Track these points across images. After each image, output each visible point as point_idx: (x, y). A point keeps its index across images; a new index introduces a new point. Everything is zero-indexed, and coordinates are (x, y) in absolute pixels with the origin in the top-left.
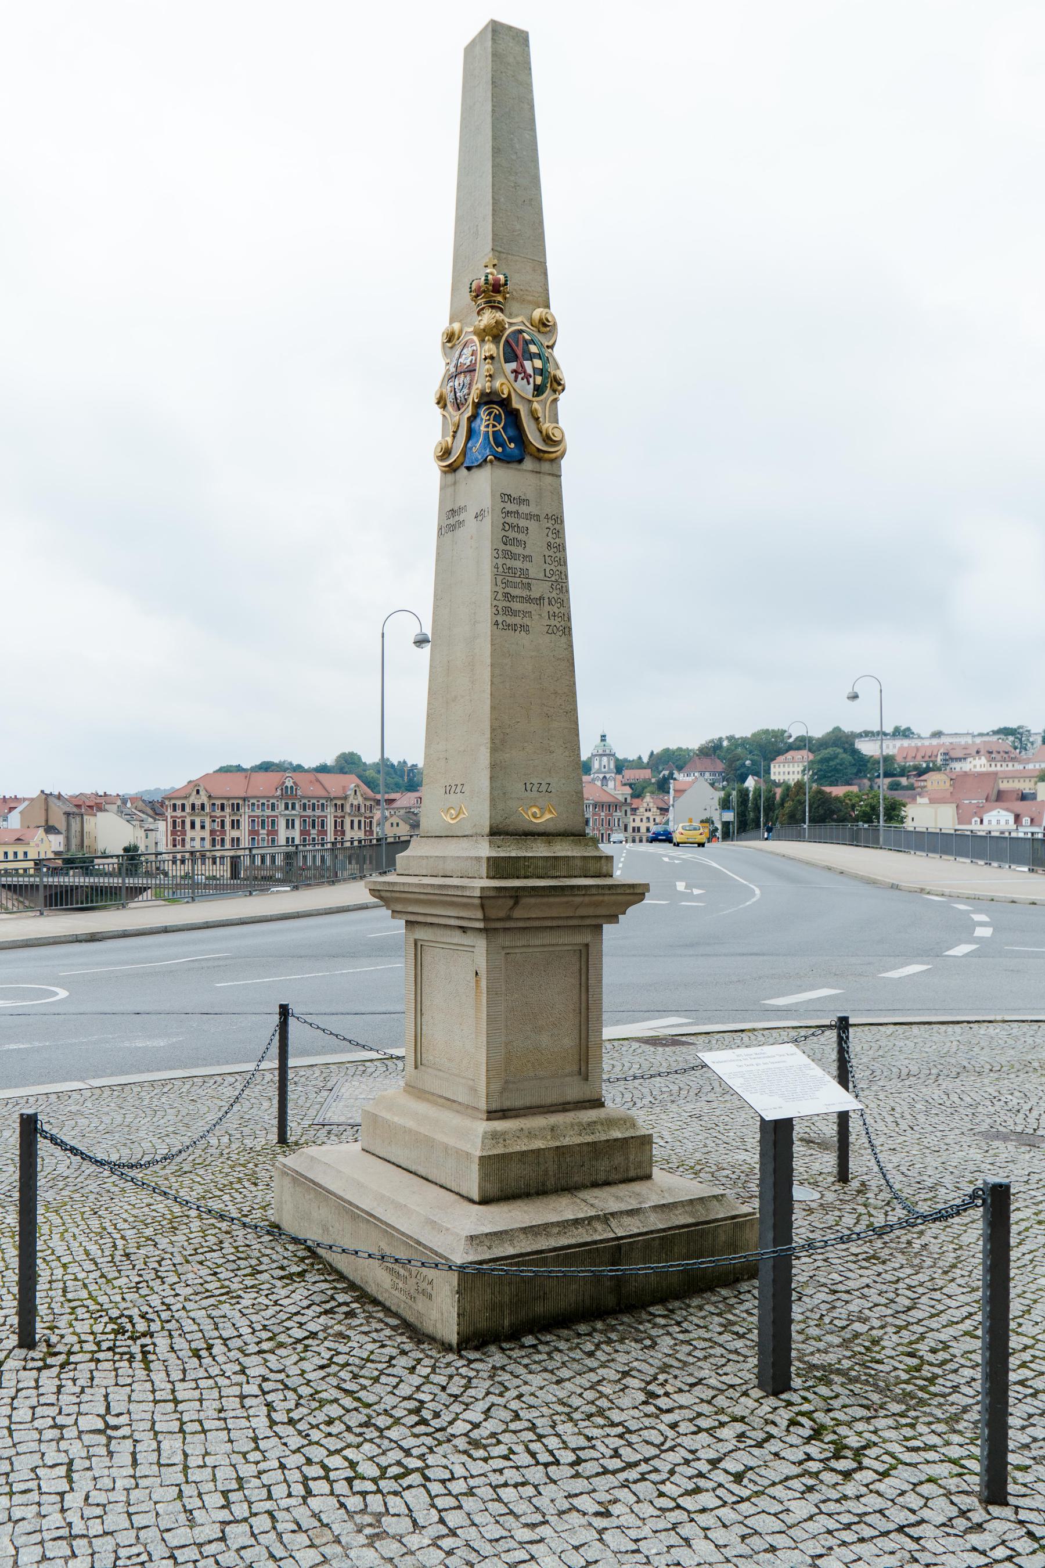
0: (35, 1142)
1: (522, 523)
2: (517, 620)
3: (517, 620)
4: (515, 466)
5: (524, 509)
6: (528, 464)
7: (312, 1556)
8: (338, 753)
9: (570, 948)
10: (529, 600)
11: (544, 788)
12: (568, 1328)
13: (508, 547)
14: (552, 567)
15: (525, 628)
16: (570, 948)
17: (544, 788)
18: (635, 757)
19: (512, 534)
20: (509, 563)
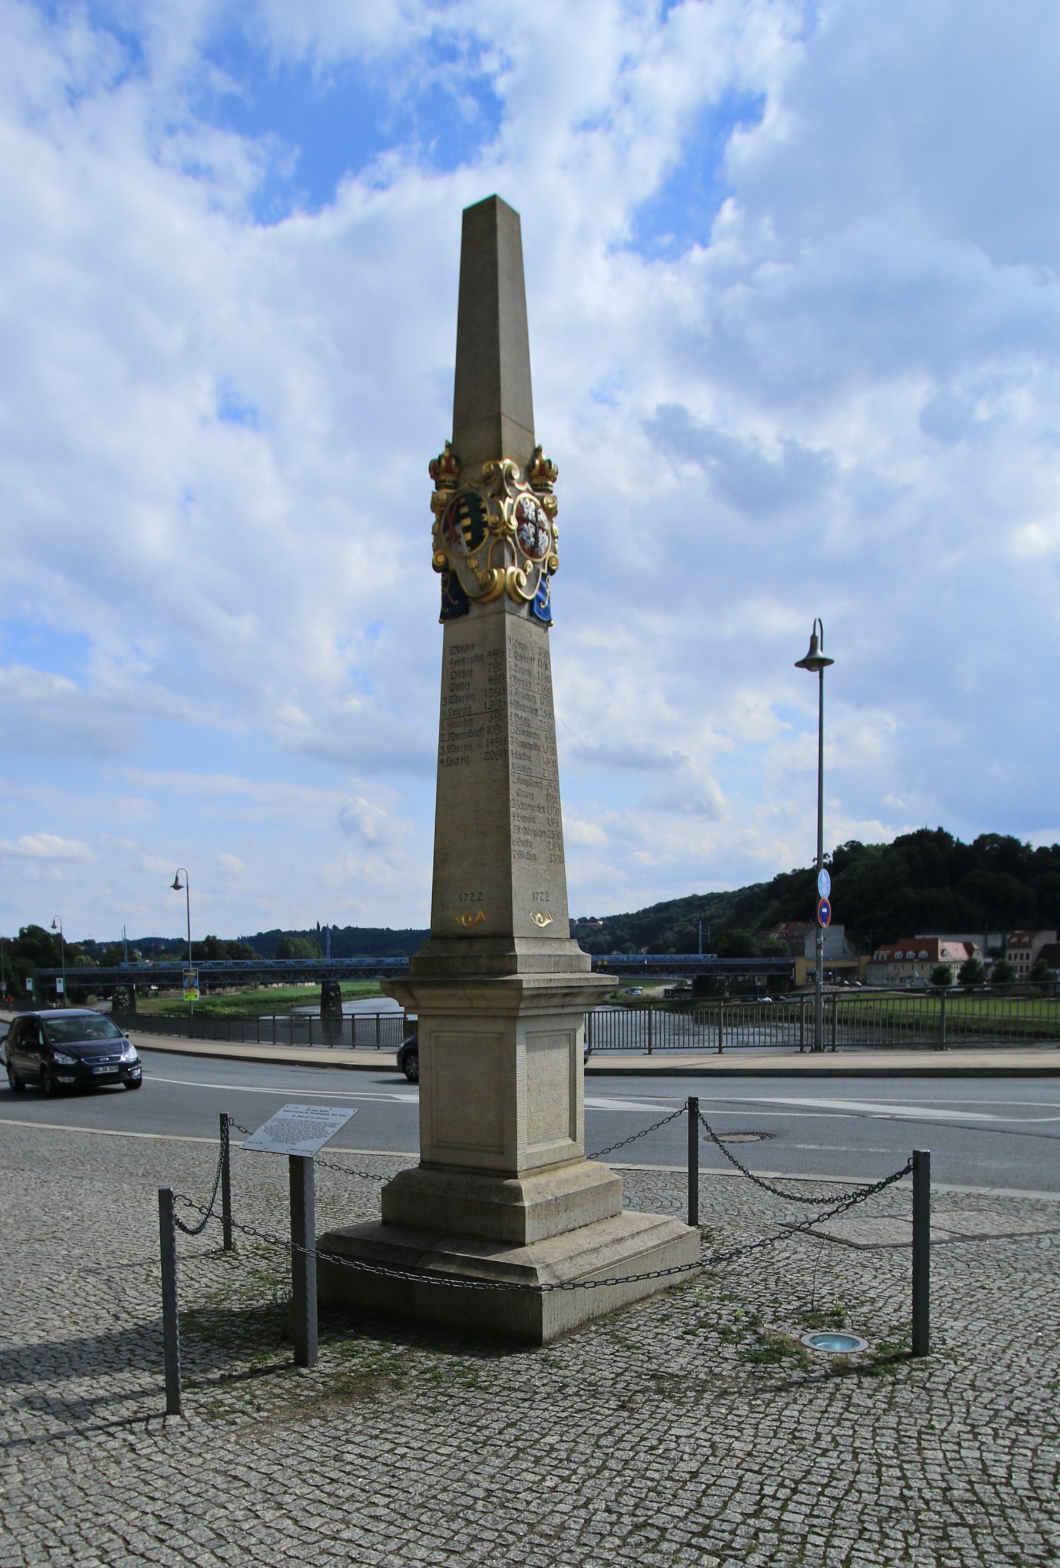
0: (224, 1213)
1: (468, 667)
2: (460, 755)
3: (460, 755)
4: (463, 617)
5: (470, 654)
6: (475, 611)
7: (65, 1561)
8: (781, 872)
9: (490, 1035)
10: (470, 734)
11: (477, 896)
12: (912, 1320)
13: (455, 693)
14: (493, 699)
15: (465, 760)
16: (490, 1035)
17: (477, 896)
18: (935, 829)
19: (458, 680)
20: (454, 706)
